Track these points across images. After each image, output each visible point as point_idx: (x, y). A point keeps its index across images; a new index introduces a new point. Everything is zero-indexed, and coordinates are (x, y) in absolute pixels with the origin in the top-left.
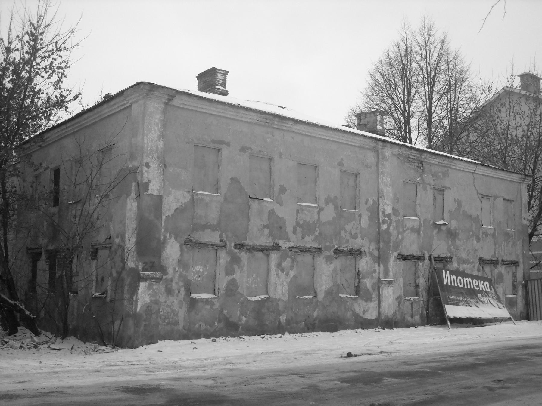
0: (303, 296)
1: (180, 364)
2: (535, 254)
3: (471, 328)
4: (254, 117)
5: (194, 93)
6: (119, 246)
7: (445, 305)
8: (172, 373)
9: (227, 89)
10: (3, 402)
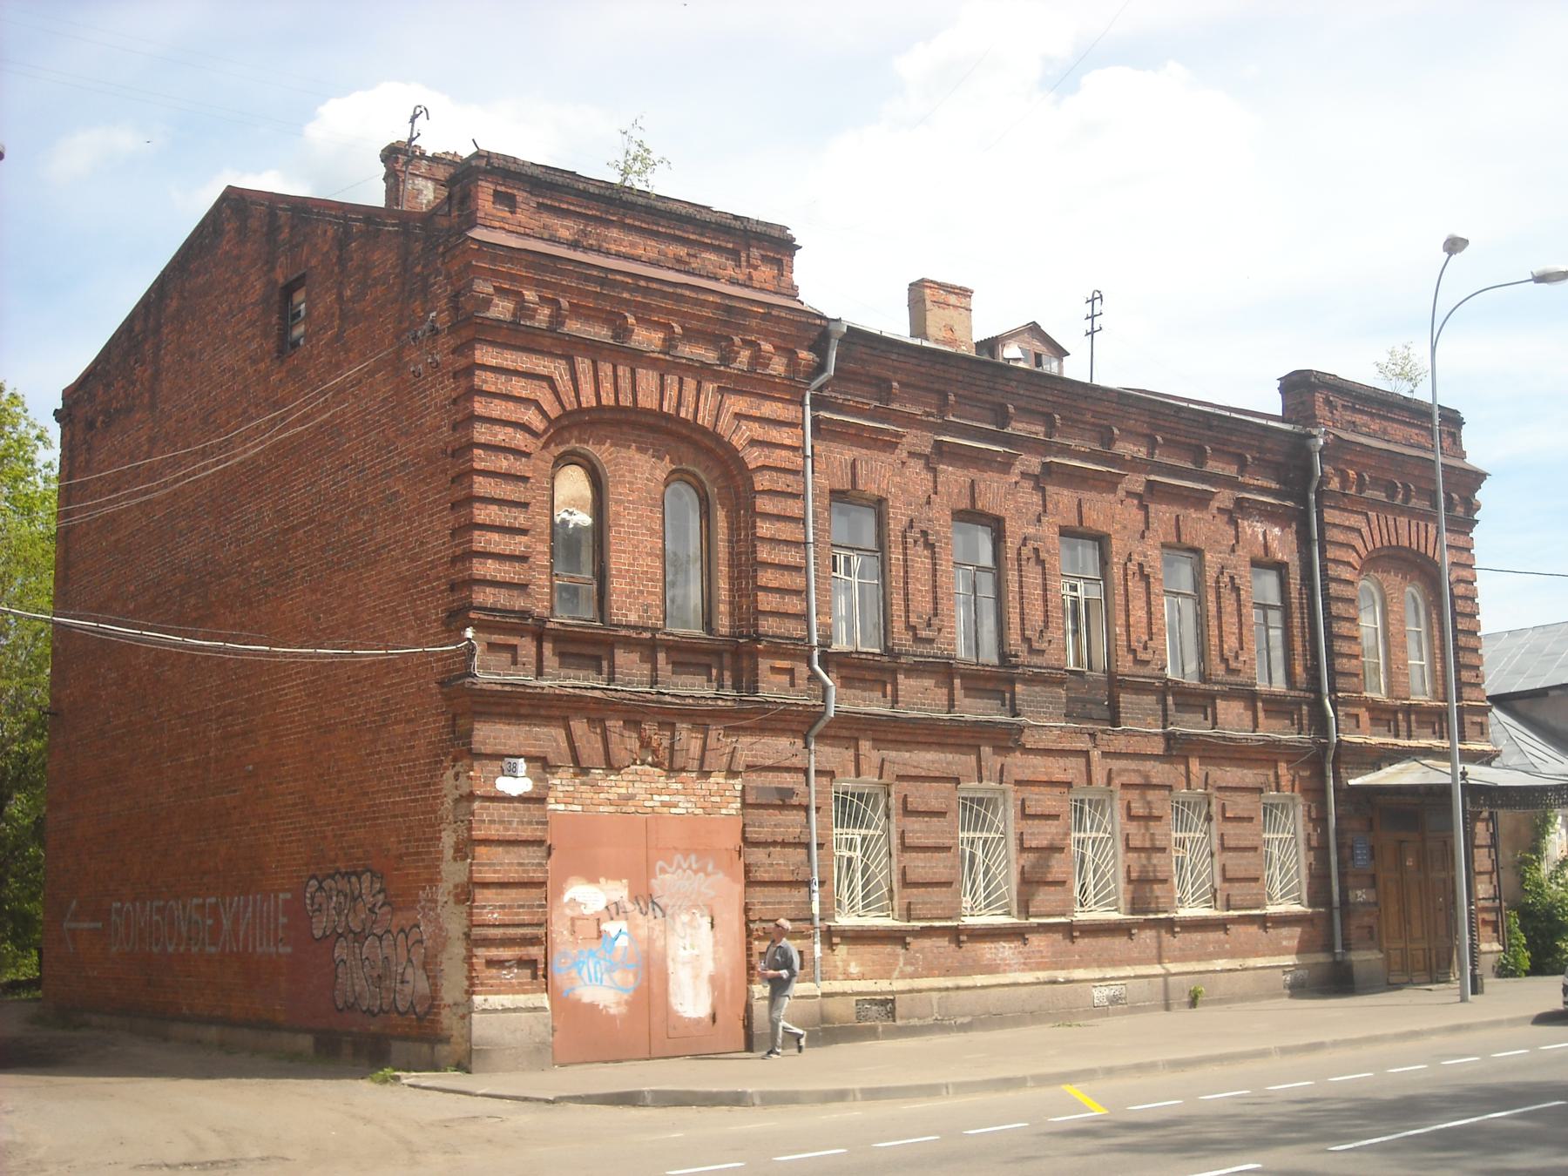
4: (1378, 453)
6: (397, 1078)
9: (1490, 983)
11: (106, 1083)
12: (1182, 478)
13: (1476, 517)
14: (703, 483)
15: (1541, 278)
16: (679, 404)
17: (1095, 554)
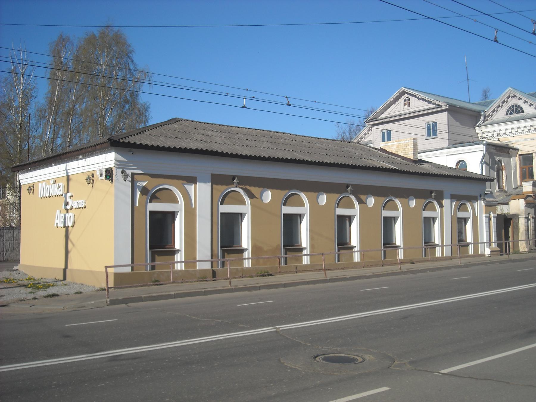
2: (443, 209)
3: (45, 169)
5: (423, 215)
7: (226, 253)
8: (436, 204)
10: (1, 290)
11: (276, 282)
12: (507, 249)
13: (379, 148)
15: (33, 195)
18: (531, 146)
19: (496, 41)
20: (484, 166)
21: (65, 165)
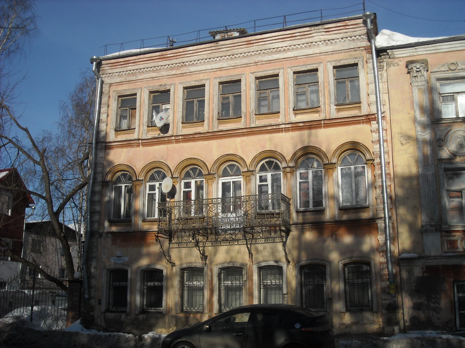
0: (382, 53)
1: (72, 242)
8: (255, 283)
14: (124, 333)
16: (447, 98)
17: (335, 204)
18: (221, 136)
19: (200, 305)
20: (325, 307)
21: (200, 42)
